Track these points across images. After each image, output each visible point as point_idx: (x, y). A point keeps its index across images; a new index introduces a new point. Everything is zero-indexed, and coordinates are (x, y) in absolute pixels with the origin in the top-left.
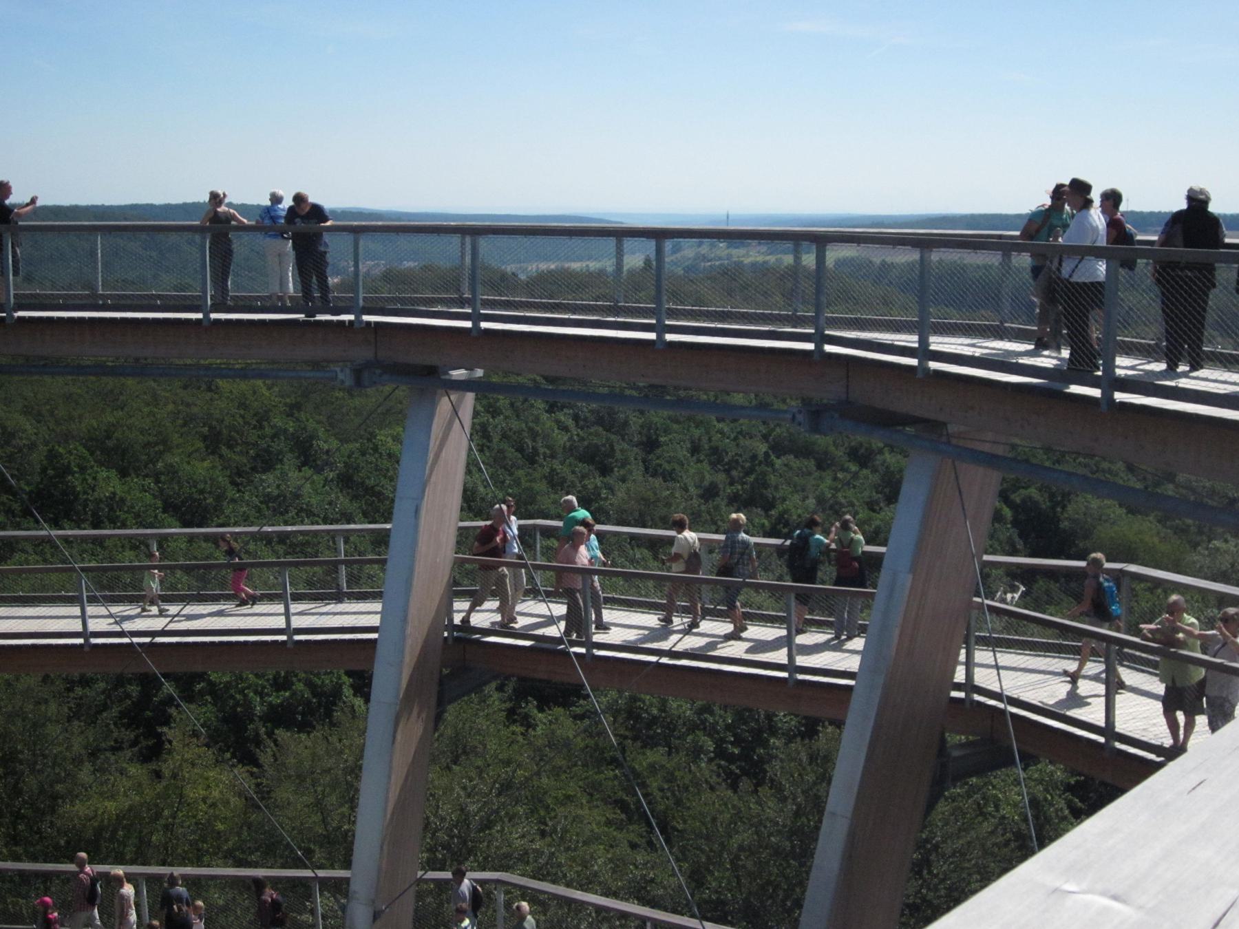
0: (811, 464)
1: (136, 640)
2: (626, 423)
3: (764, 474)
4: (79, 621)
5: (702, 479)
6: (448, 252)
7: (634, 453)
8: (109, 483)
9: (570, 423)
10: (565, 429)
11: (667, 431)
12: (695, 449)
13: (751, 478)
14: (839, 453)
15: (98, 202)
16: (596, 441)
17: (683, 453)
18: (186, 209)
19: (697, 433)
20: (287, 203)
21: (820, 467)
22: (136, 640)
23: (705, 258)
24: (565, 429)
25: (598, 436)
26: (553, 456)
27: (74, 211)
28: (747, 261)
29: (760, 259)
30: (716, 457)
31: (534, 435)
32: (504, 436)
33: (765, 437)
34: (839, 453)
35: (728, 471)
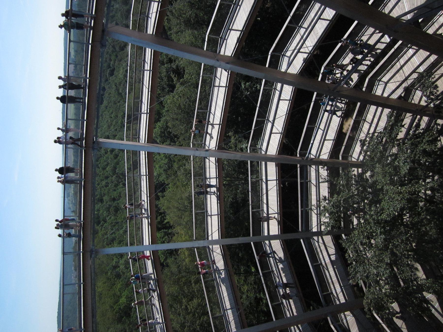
0: (118, 166)
1: (159, 10)
2: (109, 205)
3: (120, 174)
4: (155, 3)
5: (121, 187)
6: (70, 258)
7: (116, 202)
8: (123, 300)
9: (109, 217)
10: (110, 218)
11: (111, 196)
12: (115, 190)
13: (121, 177)
14: (115, 161)
15: (56, 315)
16: (113, 210)
17: (116, 192)
18: (68, 42)
19: (111, 190)
20: (60, 231)
21: (118, 164)
22: (159, 10)
23: (72, 202)
24: (110, 218)
25: (112, 209)
26: (116, 219)
27: (59, 313)
28: (73, 192)
29: (72, 189)
30: (116, 186)
31: (112, 223)
32: (112, 230)
33: (112, 176)
34: (115, 161)
35: (120, 183)
